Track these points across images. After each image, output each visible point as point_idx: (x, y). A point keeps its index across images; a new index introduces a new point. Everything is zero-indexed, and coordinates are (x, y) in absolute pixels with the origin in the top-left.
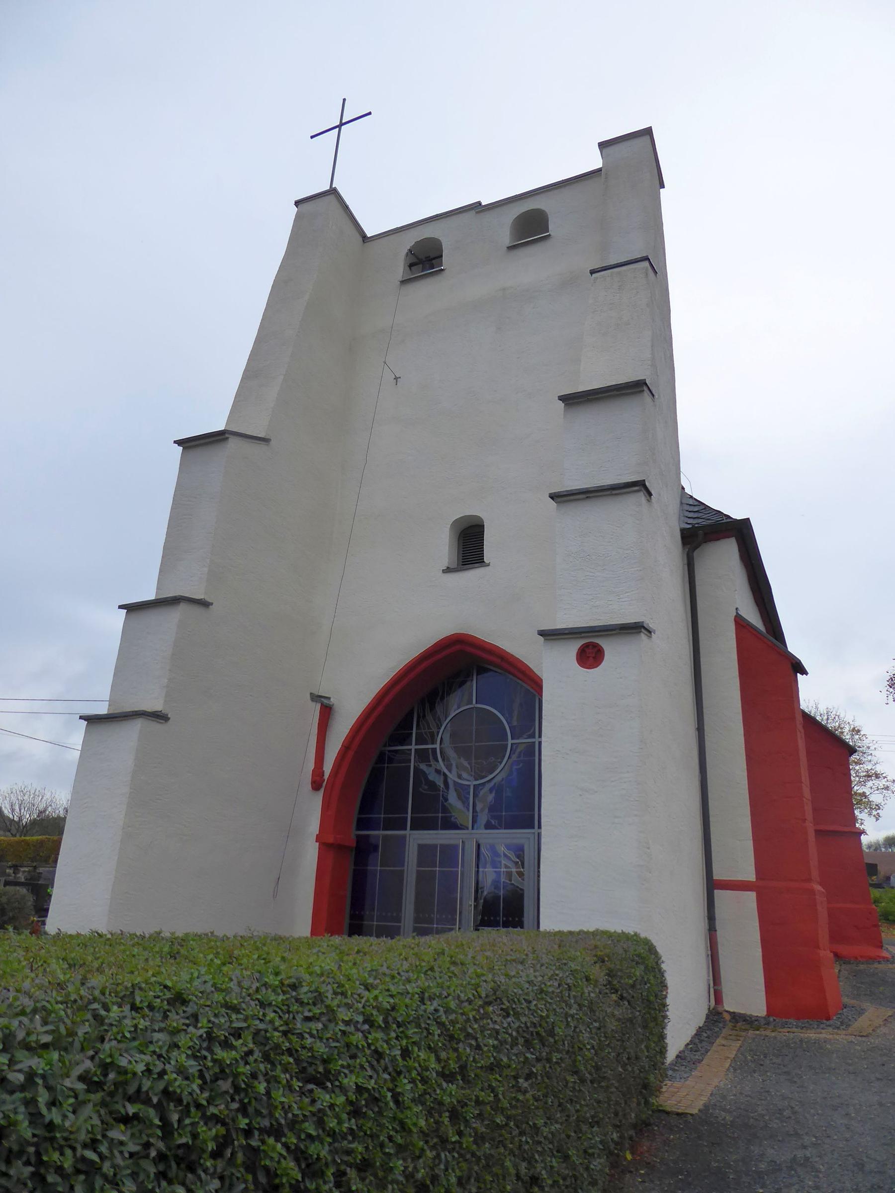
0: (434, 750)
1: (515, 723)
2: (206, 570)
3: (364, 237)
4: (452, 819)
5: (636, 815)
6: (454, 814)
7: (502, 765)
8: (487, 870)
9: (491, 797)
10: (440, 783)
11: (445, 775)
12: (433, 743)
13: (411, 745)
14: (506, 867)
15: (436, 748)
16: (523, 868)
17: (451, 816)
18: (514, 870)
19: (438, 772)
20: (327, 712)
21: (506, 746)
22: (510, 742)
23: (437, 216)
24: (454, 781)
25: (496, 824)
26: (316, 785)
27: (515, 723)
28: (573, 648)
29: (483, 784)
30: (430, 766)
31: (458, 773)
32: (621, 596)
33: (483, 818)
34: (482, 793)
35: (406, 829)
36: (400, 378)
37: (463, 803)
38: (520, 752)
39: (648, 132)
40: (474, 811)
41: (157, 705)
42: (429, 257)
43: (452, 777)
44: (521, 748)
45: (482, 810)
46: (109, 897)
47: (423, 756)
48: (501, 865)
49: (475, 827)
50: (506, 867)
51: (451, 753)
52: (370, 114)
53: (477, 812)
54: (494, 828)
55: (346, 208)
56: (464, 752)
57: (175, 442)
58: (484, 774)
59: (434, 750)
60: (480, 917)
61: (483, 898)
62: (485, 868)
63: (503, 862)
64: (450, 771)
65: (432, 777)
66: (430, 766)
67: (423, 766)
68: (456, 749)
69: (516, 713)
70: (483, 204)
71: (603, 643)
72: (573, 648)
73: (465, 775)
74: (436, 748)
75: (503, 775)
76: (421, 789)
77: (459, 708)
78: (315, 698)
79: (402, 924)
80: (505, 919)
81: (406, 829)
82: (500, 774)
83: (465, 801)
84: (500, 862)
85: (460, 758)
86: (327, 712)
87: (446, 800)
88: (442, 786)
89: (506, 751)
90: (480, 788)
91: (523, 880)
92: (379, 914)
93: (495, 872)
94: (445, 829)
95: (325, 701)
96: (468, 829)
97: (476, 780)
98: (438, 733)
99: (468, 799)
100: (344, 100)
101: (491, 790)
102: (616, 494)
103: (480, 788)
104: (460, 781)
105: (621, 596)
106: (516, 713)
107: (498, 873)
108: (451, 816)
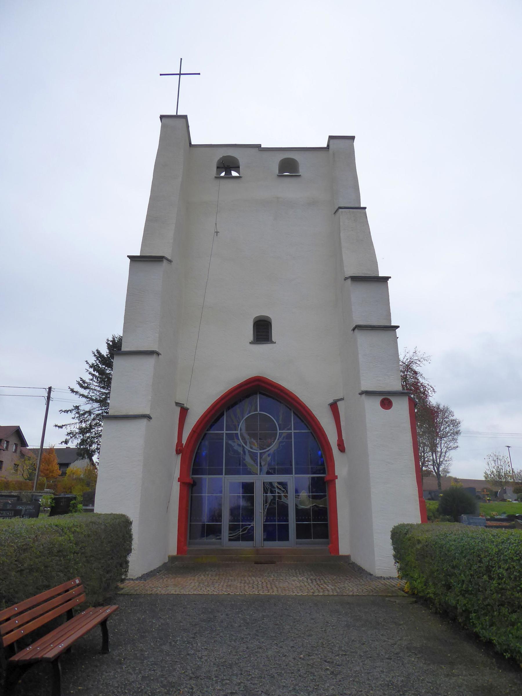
0: (237, 434)
1: (281, 422)
2: (157, 335)
3: (190, 143)
4: (248, 469)
5: (411, 474)
6: (249, 467)
7: (275, 443)
8: (268, 494)
9: (269, 459)
10: (240, 450)
11: (243, 446)
12: (235, 430)
13: (224, 431)
14: (278, 493)
15: (238, 433)
16: (287, 493)
17: (247, 468)
18: (282, 494)
19: (239, 445)
20: (184, 412)
21: (276, 433)
22: (278, 431)
23: (236, 145)
24: (249, 451)
25: (272, 472)
26: (178, 452)
27: (281, 422)
28: (379, 399)
29: (265, 452)
30: (235, 442)
31: (250, 446)
32: (390, 377)
33: (265, 469)
34: (264, 457)
35: (222, 475)
36: (219, 232)
37: (254, 461)
38: (284, 437)
39: (353, 138)
40: (261, 465)
41: (147, 412)
42: (229, 166)
43: (247, 447)
44: (284, 435)
45: (265, 465)
46: (138, 516)
47: (230, 437)
48: (275, 492)
49: (261, 473)
50: (278, 493)
51: (247, 437)
52: (199, 74)
53: (262, 466)
54: (272, 474)
55: (188, 127)
56: (253, 436)
57: (128, 256)
58: (264, 447)
59: (237, 434)
60: (265, 518)
61: (266, 508)
62: (267, 493)
63: (277, 491)
64: (246, 445)
65: (236, 447)
66: (235, 442)
67: (230, 442)
68: (249, 434)
69: (281, 417)
70: (262, 147)
71: (392, 399)
72: (379, 399)
73: (254, 447)
74: (238, 433)
75: (275, 448)
76: (229, 454)
77: (249, 413)
78: (177, 404)
79: (329, 522)
80: (275, 518)
81: (222, 475)
82: (274, 447)
83: (255, 461)
84: (275, 491)
85: (251, 439)
86: (184, 412)
87: (244, 460)
88: (242, 452)
89: (277, 436)
90: (263, 454)
91: (287, 499)
92: (278, 518)
93: (272, 495)
94: (243, 475)
95: (182, 405)
96: (257, 474)
97: (260, 450)
98: (239, 425)
99: (257, 459)
100: (181, 59)
101: (269, 455)
102: (385, 330)
103: (263, 454)
104: (252, 450)
105: (390, 377)
106: (281, 417)
107: (274, 496)
108: (247, 468)
